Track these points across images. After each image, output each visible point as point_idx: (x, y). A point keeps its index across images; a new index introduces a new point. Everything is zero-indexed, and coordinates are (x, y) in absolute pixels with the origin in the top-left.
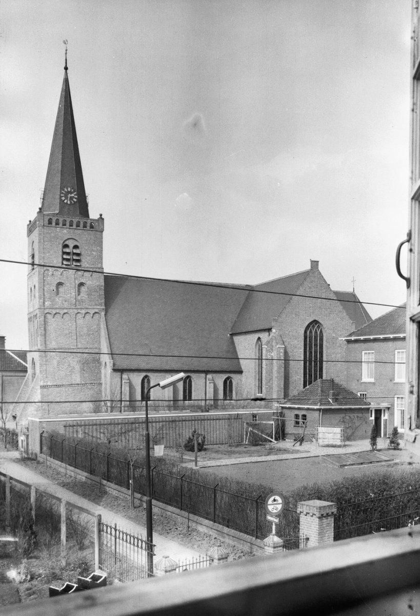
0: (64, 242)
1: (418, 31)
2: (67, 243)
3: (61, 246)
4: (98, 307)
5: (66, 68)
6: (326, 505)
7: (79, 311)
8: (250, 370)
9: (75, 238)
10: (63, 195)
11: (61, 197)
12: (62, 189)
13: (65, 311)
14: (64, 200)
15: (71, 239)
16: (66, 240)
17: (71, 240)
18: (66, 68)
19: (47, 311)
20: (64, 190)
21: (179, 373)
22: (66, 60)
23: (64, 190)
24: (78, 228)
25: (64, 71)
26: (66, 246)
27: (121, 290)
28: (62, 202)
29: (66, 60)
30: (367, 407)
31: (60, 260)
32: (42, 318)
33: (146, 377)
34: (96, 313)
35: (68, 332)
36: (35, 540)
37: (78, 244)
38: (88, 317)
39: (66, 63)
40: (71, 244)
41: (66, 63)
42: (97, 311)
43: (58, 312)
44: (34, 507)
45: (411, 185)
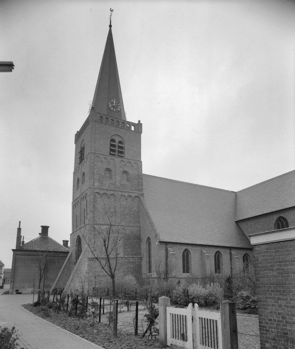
0: (111, 137)
2: (113, 138)
3: (109, 140)
4: (137, 192)
5: (110, 26)
7: (123, 194)
13: (112, 192)
14: (113, 109)
15: (117, 135)
18: (110, 26)
19: (97, 191)
21: (72, 206)
22: (111, 21)
25: (109, 28)
26: (113, 140)
29: (111, 21)
30: (186, 271)
31: (108, 150)
32: (92, 197)
33: (186, 250)
34: (136, 196)
37: (122, 141)
39: (111, 23)
40: (117, 139)
41: (111, 23)
42: (137, 195)
43: (105, 192)
44: (278, 216)
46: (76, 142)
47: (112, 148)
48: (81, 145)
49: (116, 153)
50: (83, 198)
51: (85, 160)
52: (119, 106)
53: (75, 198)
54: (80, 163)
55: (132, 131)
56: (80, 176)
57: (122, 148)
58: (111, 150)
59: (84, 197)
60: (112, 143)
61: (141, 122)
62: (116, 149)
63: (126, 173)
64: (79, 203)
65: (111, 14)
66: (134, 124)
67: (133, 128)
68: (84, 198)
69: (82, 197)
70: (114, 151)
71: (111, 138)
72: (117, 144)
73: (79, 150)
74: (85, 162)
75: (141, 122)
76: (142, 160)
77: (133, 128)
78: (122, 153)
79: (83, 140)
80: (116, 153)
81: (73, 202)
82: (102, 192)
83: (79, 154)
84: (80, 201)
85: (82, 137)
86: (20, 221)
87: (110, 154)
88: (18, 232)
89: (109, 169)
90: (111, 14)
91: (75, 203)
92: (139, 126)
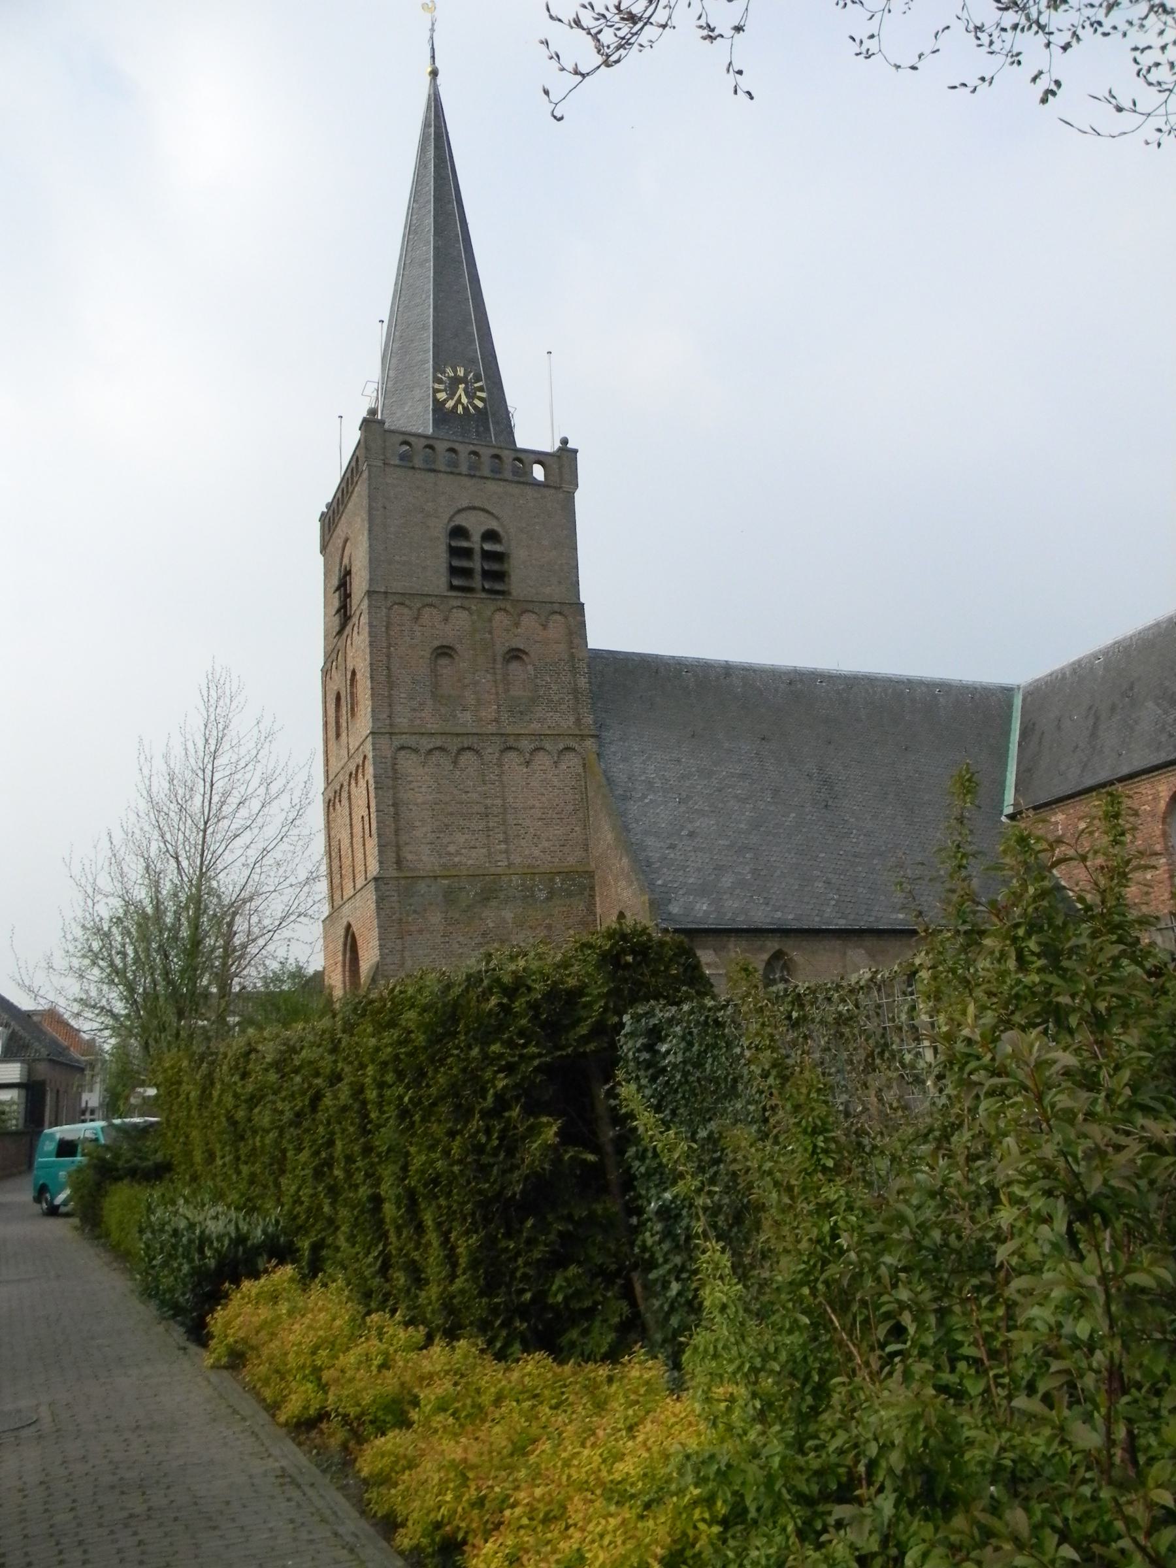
0: (451, 519)
1: (676, 931)
2: (460, 520)
6: (365, 493)
8: (870, 1229)
9: (489, 508)
10: (442, 387)
11: (436, 391)
12: (438, 368)
16: (460, 511)
17: (481, 513)
20: (444, 372)
22: (433, 49)
23: (444, 372)
24: (498, 476)
25: (428, 78)
26: (459, 532)
27: (731, 946)
28: (438, 406)
29: (433, 49)
35: (758, 1026)
36: (218, 1179)
37: (494, 525)
38: (542, 759)
45: (336, 621)
46: (324, 548)
47: (456, 563)
48: (341, 563)
49: (477, 582)
50: (357, 771)
51: (355, 620)
52: (479, 394)
53: (333, 771)
54: (340, 632)
55: (537, 484)
56: (339, 682)
57: (499, 557)
58: (454, 571)
59: (360, 770)
60: (453, 544)
61: (570, 446)
62: (477, 564)
63: (518, 658)
64: (345, 795)
65: (433, 24)
66: (540, 458)
67: (538, 472)
68: (360, 776)
69: (352, 767)
70: (467, 573)
71: (453, 524)
72: (475, 542)
73: (335, 582)
74: (356, 629)
75: (570, 446)
76: (582, 600)
77: (538, 472)
78: (500, 576)
79: (346, 540)
80: (477, 582)
81: (326, 789)
82: (426, 744)
83: (337, 594)
84: (346, 784)
85: (341, 531)
86: (562, 435)
87: (452, 588)
88: (12, 1005)
89: (519, 650)
90: (433, 24)
91: (332, 795)
92: (576, 451)
